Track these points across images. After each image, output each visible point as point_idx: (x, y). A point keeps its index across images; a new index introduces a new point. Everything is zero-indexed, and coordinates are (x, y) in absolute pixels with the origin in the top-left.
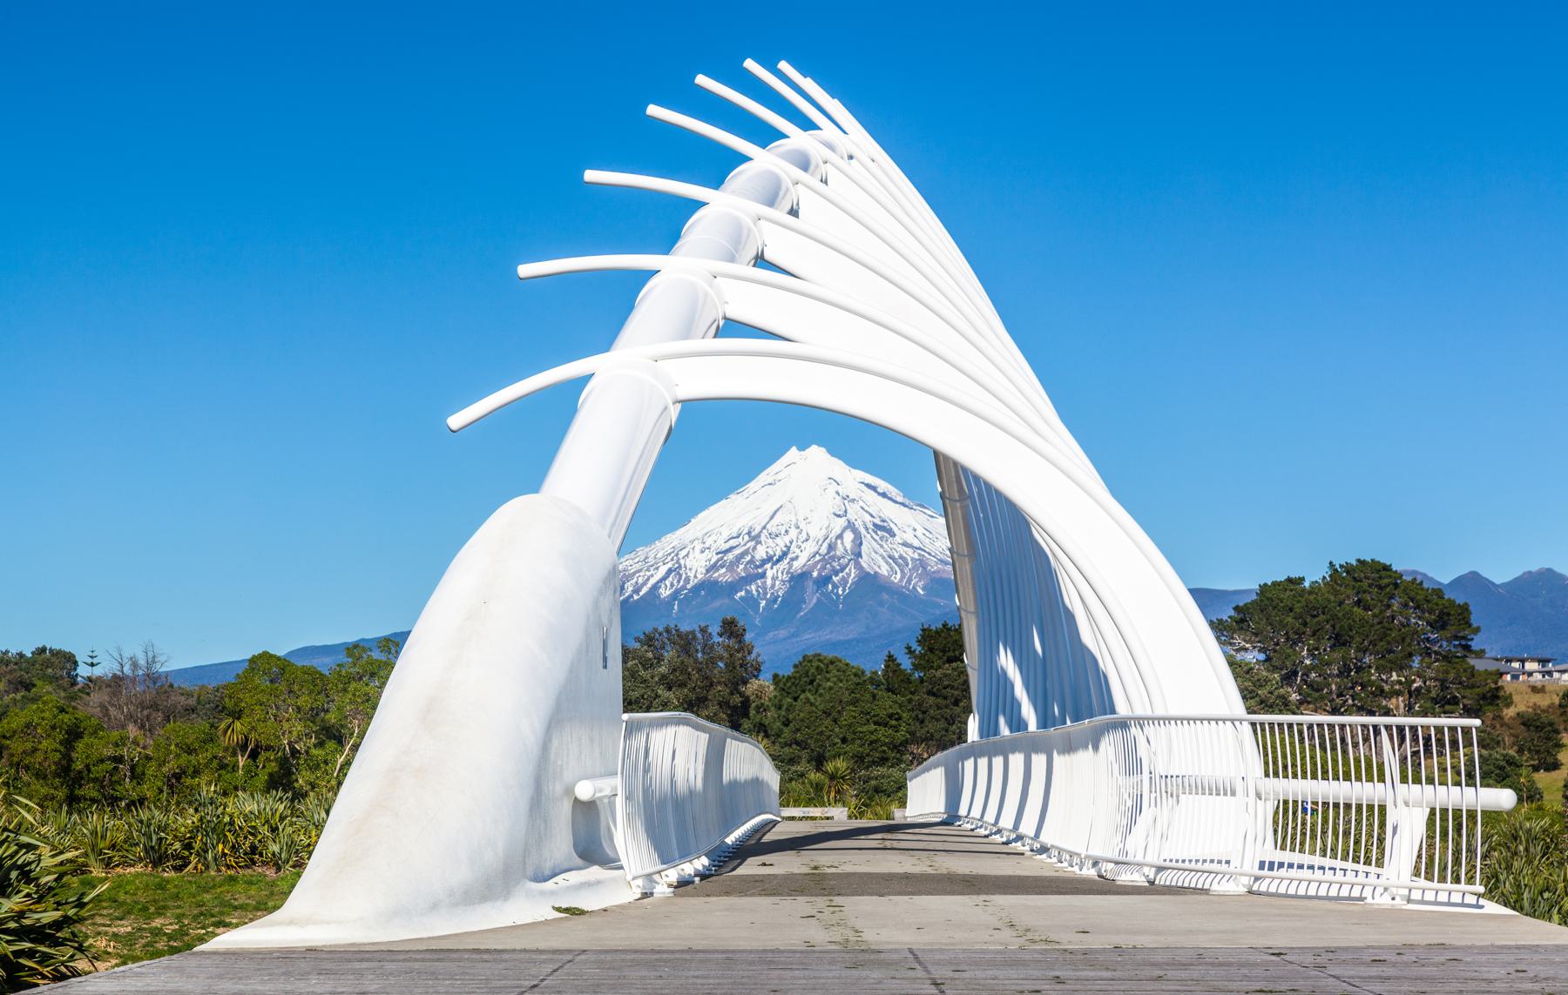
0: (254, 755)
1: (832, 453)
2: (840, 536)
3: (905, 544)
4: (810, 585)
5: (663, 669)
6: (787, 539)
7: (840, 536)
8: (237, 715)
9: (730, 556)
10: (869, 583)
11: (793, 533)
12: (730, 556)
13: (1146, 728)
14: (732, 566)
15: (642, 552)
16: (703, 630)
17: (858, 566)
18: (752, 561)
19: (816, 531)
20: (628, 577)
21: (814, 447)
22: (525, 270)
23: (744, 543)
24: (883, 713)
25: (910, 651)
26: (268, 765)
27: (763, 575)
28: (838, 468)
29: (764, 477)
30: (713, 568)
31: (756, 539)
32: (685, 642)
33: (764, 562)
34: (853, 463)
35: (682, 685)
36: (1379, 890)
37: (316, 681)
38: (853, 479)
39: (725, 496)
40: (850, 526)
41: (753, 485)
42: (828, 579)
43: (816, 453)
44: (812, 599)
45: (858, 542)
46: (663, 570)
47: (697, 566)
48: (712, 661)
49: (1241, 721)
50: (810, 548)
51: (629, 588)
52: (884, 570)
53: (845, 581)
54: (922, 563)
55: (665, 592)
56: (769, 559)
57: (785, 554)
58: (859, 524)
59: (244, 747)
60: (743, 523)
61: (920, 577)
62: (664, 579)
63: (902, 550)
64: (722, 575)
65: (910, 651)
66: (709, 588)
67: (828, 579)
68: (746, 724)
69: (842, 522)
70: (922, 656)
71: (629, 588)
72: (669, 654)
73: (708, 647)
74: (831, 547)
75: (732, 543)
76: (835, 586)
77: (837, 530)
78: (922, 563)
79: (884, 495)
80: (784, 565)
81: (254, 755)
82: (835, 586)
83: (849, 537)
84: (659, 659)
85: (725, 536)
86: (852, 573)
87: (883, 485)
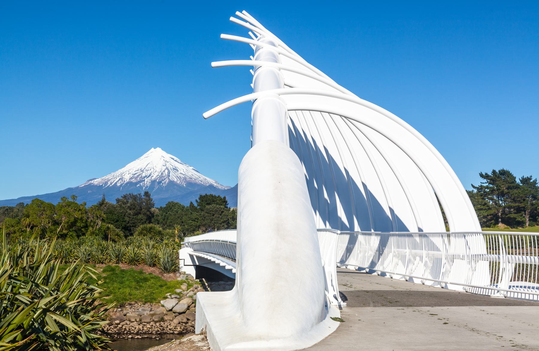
0: (32, 228)
1: (163, 150)
2: (164, 171)
3: (181, 173)
4: (156, 184)
5: (129, 205)
6: (150, 171)
7: (164, 171)
8: (28, 216)
9: (136, 175)
10: (172, 183)
11: (152, 170)
12: (136, 175)
13: (466, 238)
14: (136, 178)
15: (113, 174)
16: (139, 195)
17: (169, 179)
18: (141, 177)
19: (158, 170)
20: (109, 180)
21: (158, 148)
22: (214, 64)
23: (139, 172)
24: (194, 218)
25: (197, 201)
26: (37, 230)
27: (144, 181)
28: (164, 153)
29: (145, 155)
30: (131, 178)
31: (143, 171)
32: (135, 198)
33: (144, 177)
34: (168, 152)
35: (134, 209)
36: (496, 291)
37: (52, 207)
38: (168, 156)
39: (135, 160)
40: (167, 168)
41: (142, 157)
42: (161, 182)
43: (159, 149)
44: (157, 187)
45: (169, 172)
46: (118, 179)
47: (127, 178)
48: (142, 203)
49: (480, 233)
50: (156, 174)
51: (109, 183)
52: (175, 180)
53: (165, 182)
54: (185, 178)
55: (118, 184)
56: (146, 176)
57: (150, 175)
58: (169, 168)
59: (29, 226)
60: (139, 167)
61: (185, 182)
62: (118, 181)
63: (180, 175)
64: (134, 180)
65: (197, 201)
66: (130, 183)
67: (161, 182)
68: (153, 220)
69: (165, 167)
70: (200, 203)
71: (109, 183)
72: (130, 201)
73: (140, 199)
74: (162, 174)
75: (136, 172)
76: (163, 184)
77: (164, 170)
78: (185, 178)
79: (176, 161)
80: (150, 178)
81: (32, 228)
82: (163, 184)
83: (166, 171)
84: (128, 202)
85: (135, 170)
86: (167, 180)
87: (175, 158)
